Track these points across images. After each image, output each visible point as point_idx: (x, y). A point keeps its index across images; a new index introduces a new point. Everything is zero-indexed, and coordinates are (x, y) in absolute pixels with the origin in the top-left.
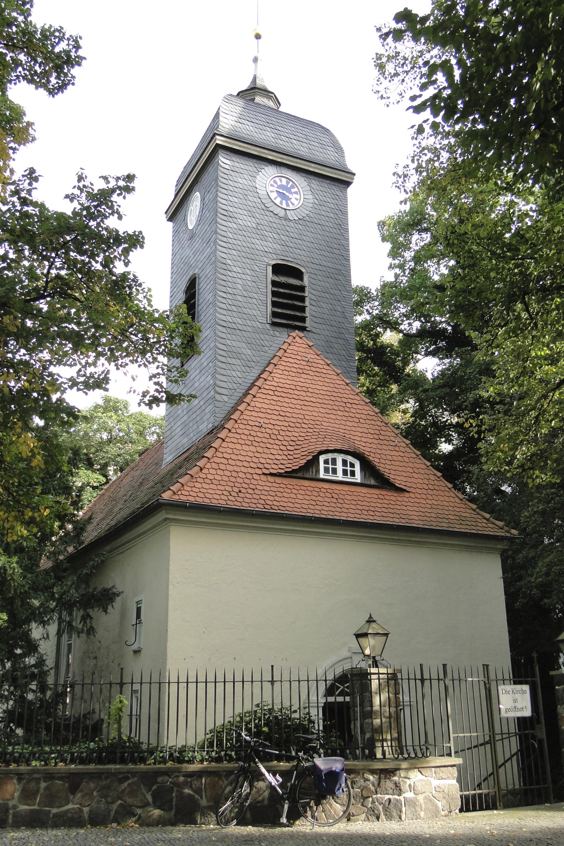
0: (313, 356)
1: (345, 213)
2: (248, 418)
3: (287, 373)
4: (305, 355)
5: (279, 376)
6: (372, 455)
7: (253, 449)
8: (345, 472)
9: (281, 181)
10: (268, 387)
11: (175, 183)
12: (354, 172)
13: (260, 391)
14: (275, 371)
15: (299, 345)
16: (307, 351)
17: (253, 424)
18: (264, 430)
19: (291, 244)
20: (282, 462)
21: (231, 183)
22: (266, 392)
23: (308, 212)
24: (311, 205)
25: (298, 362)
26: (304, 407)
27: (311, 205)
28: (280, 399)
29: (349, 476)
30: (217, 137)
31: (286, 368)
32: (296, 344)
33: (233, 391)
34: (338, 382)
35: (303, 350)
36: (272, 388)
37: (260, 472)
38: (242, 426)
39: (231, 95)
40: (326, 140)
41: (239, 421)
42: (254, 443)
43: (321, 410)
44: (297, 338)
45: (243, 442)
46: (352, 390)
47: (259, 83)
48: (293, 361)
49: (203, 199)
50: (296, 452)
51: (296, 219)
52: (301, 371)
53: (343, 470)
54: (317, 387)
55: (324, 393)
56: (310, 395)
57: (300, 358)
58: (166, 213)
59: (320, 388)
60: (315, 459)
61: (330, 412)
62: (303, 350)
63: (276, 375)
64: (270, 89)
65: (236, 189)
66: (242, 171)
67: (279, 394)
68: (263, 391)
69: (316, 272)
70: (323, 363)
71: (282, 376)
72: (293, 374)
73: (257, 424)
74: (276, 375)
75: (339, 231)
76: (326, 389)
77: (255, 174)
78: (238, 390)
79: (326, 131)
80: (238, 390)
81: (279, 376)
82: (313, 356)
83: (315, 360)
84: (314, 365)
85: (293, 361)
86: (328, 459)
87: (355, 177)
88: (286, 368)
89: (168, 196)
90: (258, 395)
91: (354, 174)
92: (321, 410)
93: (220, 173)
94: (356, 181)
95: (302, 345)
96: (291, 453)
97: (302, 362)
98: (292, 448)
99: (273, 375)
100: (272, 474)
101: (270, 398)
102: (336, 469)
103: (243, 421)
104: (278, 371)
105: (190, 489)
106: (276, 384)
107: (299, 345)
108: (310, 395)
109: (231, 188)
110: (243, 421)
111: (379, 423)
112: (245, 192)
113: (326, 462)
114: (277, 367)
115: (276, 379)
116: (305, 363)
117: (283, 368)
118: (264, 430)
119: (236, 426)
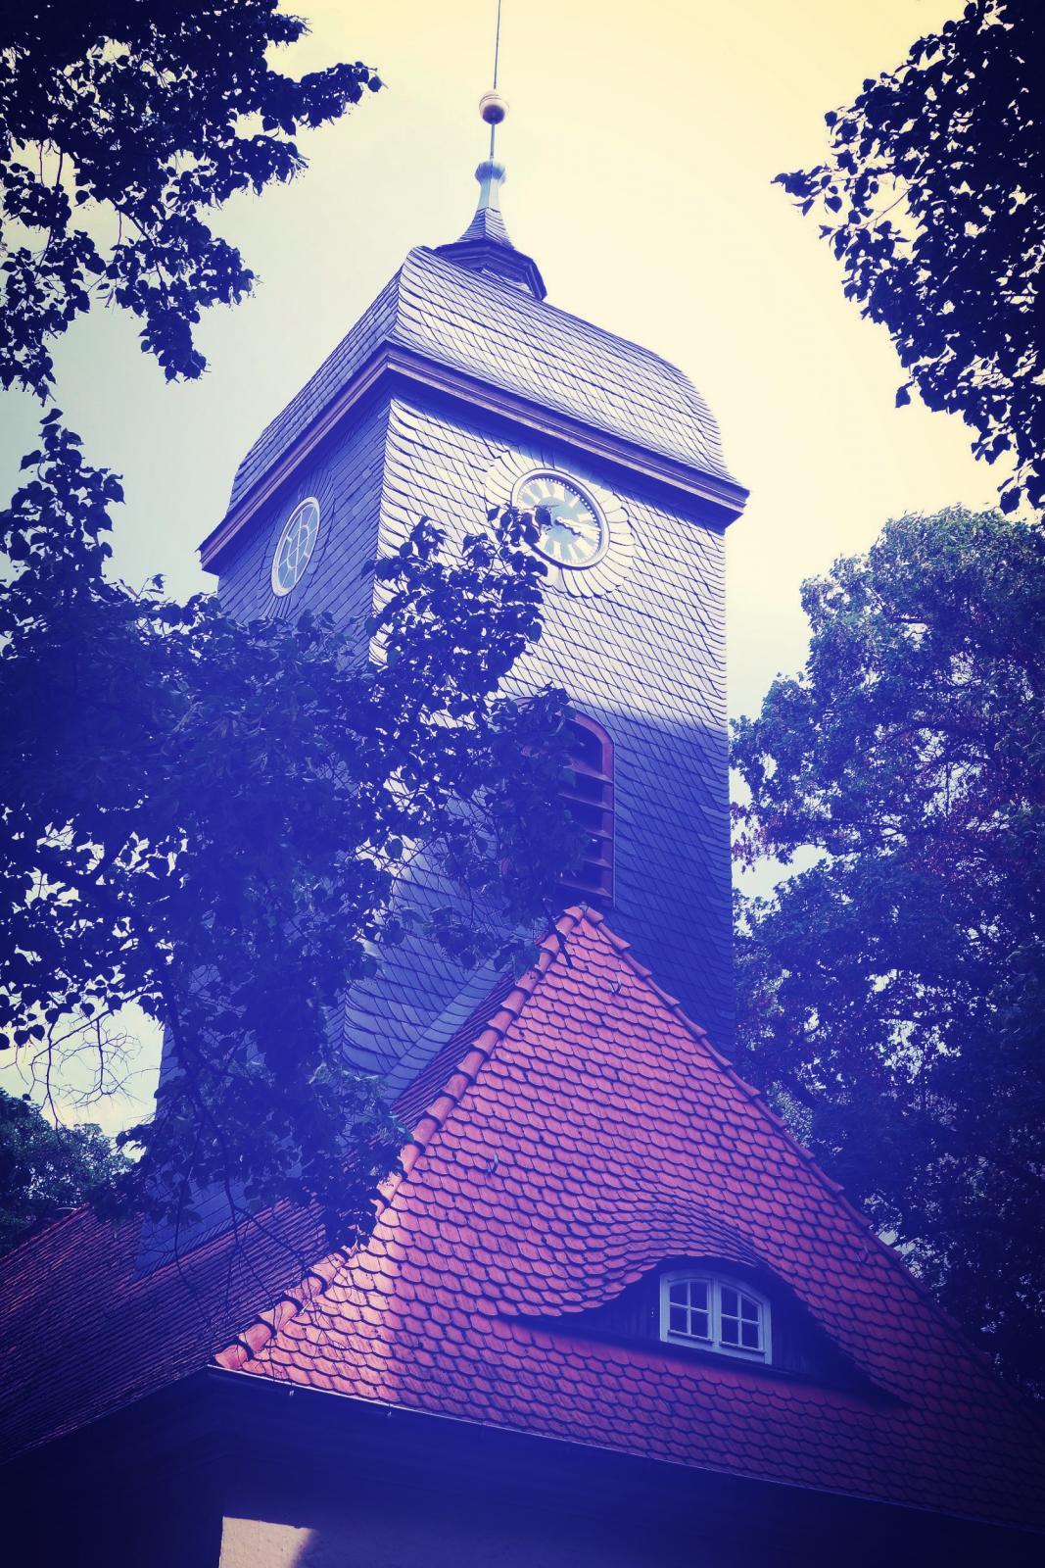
0: (628, 981)
1: (715, 592)
2: (454, 1143)
3: (559, 1022)
4: (606, 973)
5: (539, 1029)
6: (801, 1284)
7: (466, 1235)
8: (729, 1331)
9: (552, 491)
10: (508, 1058)
11: (234, 471)
12: (745, 485)
13: (485, 1068)
14: (526, 1012)
15: (589, 944)
16: (614, 963)
17: (469, 1161)
18: (498, 1184)
19: (572, 662)
20: (554, 1283)
21: (419, 478)
22: (503, 1071)
23: (619, 581)
24: (629, 562)
25: (588, 992)
26: (608, 1127)
27: (629, 562)
28: (543, 1095)
29: (689, 1333)
30: (391, 354)
31: (558, 1007)
32: (582, 941)
33: (392, 1062)
34: (698, 1060)
35: (601, 960)
36: (520, 1061)
37: (490, 1309)
38: (436, 1166)
39: (425, 249)
40: (672, 393)
41: (430, 1151)
42: (473, 1221)
43: (656, 1138)
44: (584, 924)
45: (441, 1214)
46: (739, 1088)
47: (491, 229)
48: (574, 988)
49: (329, 517)
50: (592, 1257)
51: (589, 594)
52: (596, 1020)
53: (724, 1321)
54: (642, 1069)
55: (663, 1089)
56: (624, 1091)
57: (593, 981)
58: (202, 548)
59: (650, 1073)
60: (650, 1283)
61: (678, 1145)
62: (601, 960)
63: (530, 1024)
64: (521, 246)
65: (431, 498)
66: (449, 450)
67: (538, 1080)
68: (495, 1067)
69: (635, 745)
70: (657, 1002)
71: (547, 1030)
72: (577, 1027)
73: (482, 1164)
74: (530, 1024)
75: (699, 639)
76: (665, 1076)
77: (484, 464)
78: (406, 1060)
79: (671, 371)
80: (406, 1060)
81: (539, 1029)
82: (628, 981)
83: (634, 993)
84: (631, 1005)
85: (574, 988)
86: (684, 1287)
87: (748, 501)
88: (558, 1007)
89: (211, 507)
90: (481, 1079)
91: (745, 493)
92: (656, 1138)
93: (390, 449)
94: (751, 509)
95: (598, 946)
96: (578, 1259)
97: (599, 994)
98: (579, 1245)
99: (521, 1023)
100: (522, 1321)
101: (514, 1088)
102: (705, 1316)
103: (441, 1152)
104: (535, 1013)
105: (291, 1345)
106: (529, 1051)
107: (589, 944)
108: (624, 1091)
109: (418, 493)
110: (441, 1152)
111: (816, 1193)
112: (457, 508)
113: (677, 1295)
114: (532, 1001)
115: (531, 1038)
116: (605, 998)
117: (547, 1005)
118: (498, 1184)
119: (422, 1163)
